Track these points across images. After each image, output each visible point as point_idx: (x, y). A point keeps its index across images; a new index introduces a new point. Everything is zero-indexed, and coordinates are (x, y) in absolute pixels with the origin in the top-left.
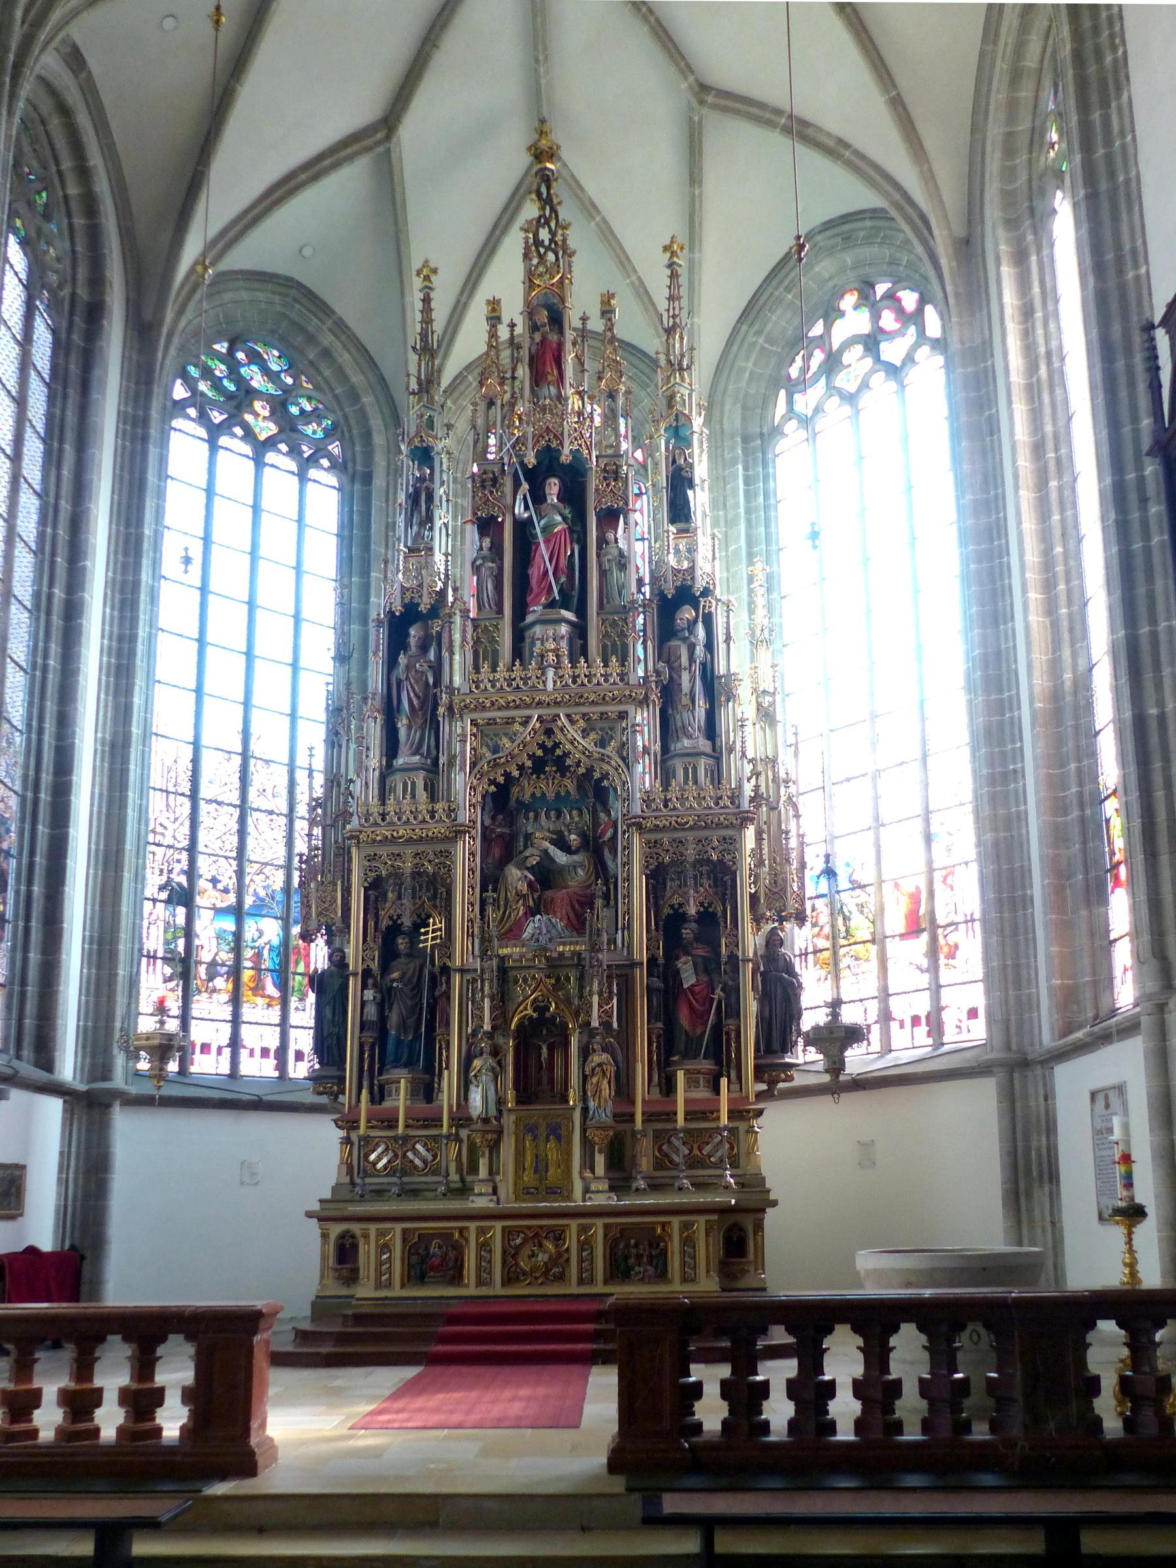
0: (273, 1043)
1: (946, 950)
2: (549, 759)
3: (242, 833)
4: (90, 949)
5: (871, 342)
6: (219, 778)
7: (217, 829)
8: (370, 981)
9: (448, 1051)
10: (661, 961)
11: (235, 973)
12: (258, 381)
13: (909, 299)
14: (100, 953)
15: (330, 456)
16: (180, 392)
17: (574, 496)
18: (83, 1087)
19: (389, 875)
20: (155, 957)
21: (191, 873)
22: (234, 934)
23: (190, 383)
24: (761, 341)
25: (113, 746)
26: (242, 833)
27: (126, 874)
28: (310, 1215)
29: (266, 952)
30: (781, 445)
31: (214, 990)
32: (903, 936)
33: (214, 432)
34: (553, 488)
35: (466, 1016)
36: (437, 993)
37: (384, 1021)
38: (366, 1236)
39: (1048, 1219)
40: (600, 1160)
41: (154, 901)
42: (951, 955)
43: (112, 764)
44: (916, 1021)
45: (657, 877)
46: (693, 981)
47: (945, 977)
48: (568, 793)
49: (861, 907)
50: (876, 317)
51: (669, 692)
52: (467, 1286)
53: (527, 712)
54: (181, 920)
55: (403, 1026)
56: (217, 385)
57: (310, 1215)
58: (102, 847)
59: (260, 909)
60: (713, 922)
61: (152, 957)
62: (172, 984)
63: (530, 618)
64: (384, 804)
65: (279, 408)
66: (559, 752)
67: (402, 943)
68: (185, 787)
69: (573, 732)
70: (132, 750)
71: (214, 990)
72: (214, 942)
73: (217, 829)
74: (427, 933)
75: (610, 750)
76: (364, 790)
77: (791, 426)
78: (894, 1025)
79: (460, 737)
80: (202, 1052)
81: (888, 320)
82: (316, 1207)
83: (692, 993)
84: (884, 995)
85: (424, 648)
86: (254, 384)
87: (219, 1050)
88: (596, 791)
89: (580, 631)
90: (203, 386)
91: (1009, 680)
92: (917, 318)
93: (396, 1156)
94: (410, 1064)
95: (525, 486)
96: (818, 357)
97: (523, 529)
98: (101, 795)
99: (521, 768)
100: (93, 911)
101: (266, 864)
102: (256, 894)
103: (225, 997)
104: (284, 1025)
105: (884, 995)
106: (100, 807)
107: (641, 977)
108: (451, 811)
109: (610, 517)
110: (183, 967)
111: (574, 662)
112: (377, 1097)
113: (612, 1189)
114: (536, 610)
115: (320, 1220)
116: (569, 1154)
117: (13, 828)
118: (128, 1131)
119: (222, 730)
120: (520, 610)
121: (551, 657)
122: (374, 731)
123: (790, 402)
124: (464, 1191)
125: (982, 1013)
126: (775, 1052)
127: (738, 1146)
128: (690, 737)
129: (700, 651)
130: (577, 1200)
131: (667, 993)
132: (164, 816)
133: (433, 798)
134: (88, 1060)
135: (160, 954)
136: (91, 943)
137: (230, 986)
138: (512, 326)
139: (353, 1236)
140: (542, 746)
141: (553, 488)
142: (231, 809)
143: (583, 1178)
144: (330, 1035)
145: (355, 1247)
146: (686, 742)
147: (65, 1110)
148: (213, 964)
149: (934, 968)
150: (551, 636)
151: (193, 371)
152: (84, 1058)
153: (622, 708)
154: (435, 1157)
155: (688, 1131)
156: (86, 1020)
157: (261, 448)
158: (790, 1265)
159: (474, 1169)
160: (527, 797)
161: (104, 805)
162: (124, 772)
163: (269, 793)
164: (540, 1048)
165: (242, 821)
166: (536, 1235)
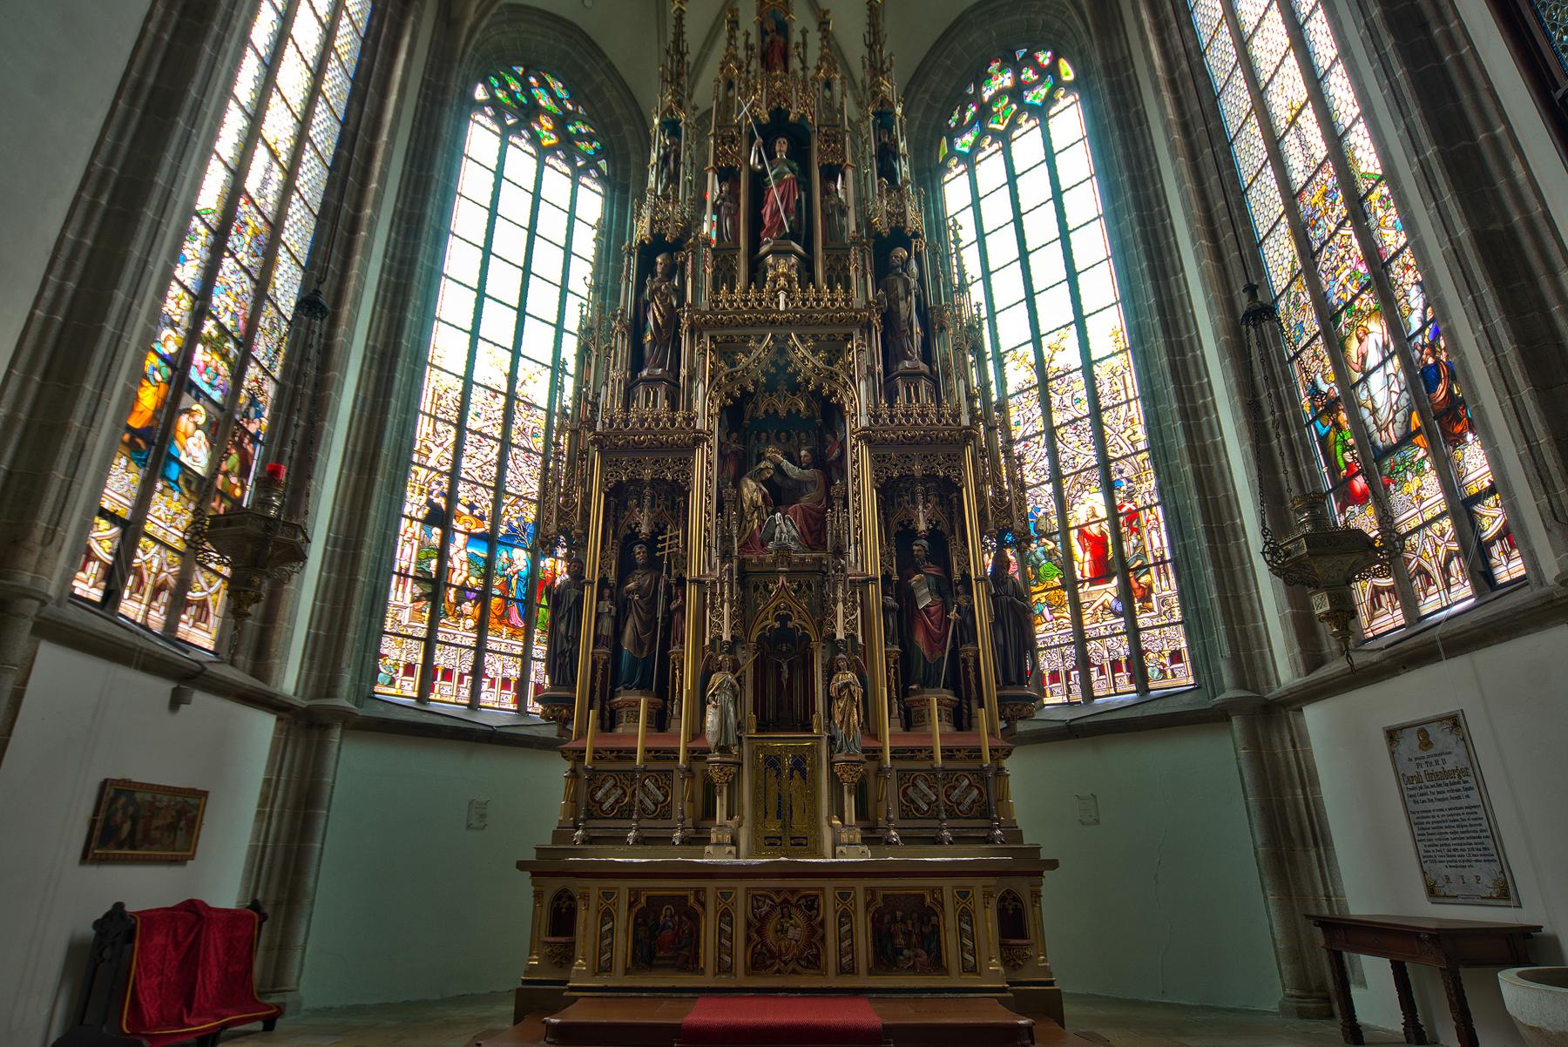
0: (514, 673)
1: (1139, 592)
3: (502, 465)
4: (333, 552)
5: (1016, 92)
6: (485, 413)
7: (479, 459)
8: (607, 592)
9: (682, 672)
10: (896, 578)
11: (483, 597)
12: (545, 101)
13: (1044, 58)
14: (343, 556)
15: (598, 169)
16: (480, 93)
17: (800, 154)
18: (305, 703)
19: (630, 481)
20: (406, 576)
21: (451, 496)
22: (485, 560)
23: (490, 89)
24: (927, 97)
25: (383, 354)
26: (502, 465)
27: (379, 478)
28: (522, 865)
29: (514, 582)
31: (461, 615)
32: (1093, 582)
33: (505, 134)
36: (673, 606)
37: (615, 635)
38: (585, 897)
39: (1322, 892)
40: (850, 803)
41: (412, 519)
42: (1146, 598)
43: (380, 371)
44: (1116, 666)
45: (889, 493)
46: (928, 601)
47: (1143, 620)
48: (799, 411)
49: (1049, 555)
50: (1017, 73)
52: (702, 972)
53: (762, 331)
54: (436, 540)
55: (638, 643)
56: (511, 95)
57: (522, 865)
58: (359, 449)
59: (511, 540)
60: (944, 542)
61: (404, 575)
62: (421, 604)
63: (764, 249)
64: (628, 411)
65: (560, 123)
66: (790, 370)
67: (639, 553)
68: (453, 416)
69: (802, 351)
70: (400, 361)
71: (461, 615)
72: (465, 567)
73: (479, 459)
74: (664, 540)
75: (836, 368)
76: (610, 398)
78: (1094, 671)
79: (696, 356)
80: (443, 679)
81: (1028, 75)
82: (531, 856)
83: (927, 612)
84: (1080, 639)
85: (669, 275)
86: (542, 102)
87: (461, 676)
89: (807, 266)
90: (500, 94)
91: (1186, 323)
92: (1053, 69)
93: (625, 794)
94: (644, 686)
95: (759, 140)
98: (365, 399)
99: (755, 383)
100: (341, 512)
101: (521, 497)
102: (509, 524)
103: (470, 623)
104: (526, 658)
105: (1080, 639)
106: (362, 410)
108: (689, 420)
110: (434, 587)
111: (804, 288)
112: (607, 724)
113: (865, 841)
115: (534, 874)
116: (814, 797)
117: (266, 413)
118: (351, 764)
119: (491, 368)
120: (755, 243)
121: (782, 281)
122: (622, 345)
123: (951, 144)
124: (698, 839)
125: (1186, 656)
126: (1012, 684)
128: (910, 359)
129: (913, 282)
131: (903, 615)
132: (431, 442)
133: (674, 407)
134: (314, 673)
135: (411, 573)
136: (335, 545)
137: (477, 613)
138: (748, 34)
139: (571, 898)
140: (774, 364)
141: (781, 147)
142: (492, 442)
143: (831, 825)
144: (563, 652)
145: (572, 912)
146: (907, 363)
147: (278, 730)
148: (462, 588)
149: (1130, 615)
150: (782, 267)
151: (493, 81)
152: (310, 670)
153: (847, 330)
154: (666, 796)
155: (943, 769)
156: (318, 628)
157: (542, 154)
159: (709, 813)
160: (761, 413)
161: (367, 408)
162: (390, 379)
163: (529, 432)
164: (779, 666)
165: (503, 456)
166: (786, 901)
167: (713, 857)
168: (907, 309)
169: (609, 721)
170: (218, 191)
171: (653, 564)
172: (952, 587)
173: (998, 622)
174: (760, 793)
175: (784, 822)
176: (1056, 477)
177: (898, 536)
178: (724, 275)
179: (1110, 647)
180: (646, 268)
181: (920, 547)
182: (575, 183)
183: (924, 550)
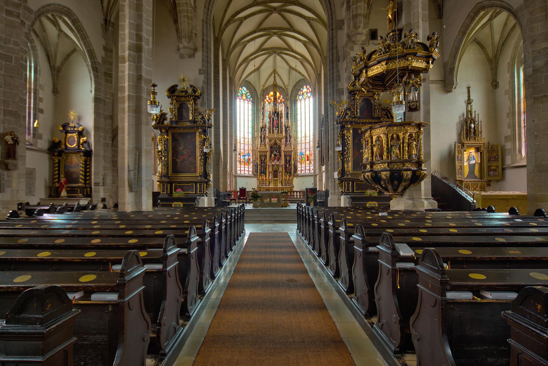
2: (275, 144)
35: (269, 169)
45: (285, 156)
51: (286, 137)
60: (290, 161)
79: (267, 140)
97: (273, 119)
109: (281, 118)
110: (240, 161)
127: (292, 183)
131: (286, 168)
141: (276, 114)
150: (276, 131)
157: (244, 100)
158: (294, 189)
168: (288, 136)
172: (290, 165)
175: (275, 184)
176: (305, 149)
177: (286, 160)
178: (270, 132)
179: (308, 168)
180: (262, 130)
183: (288, 162)
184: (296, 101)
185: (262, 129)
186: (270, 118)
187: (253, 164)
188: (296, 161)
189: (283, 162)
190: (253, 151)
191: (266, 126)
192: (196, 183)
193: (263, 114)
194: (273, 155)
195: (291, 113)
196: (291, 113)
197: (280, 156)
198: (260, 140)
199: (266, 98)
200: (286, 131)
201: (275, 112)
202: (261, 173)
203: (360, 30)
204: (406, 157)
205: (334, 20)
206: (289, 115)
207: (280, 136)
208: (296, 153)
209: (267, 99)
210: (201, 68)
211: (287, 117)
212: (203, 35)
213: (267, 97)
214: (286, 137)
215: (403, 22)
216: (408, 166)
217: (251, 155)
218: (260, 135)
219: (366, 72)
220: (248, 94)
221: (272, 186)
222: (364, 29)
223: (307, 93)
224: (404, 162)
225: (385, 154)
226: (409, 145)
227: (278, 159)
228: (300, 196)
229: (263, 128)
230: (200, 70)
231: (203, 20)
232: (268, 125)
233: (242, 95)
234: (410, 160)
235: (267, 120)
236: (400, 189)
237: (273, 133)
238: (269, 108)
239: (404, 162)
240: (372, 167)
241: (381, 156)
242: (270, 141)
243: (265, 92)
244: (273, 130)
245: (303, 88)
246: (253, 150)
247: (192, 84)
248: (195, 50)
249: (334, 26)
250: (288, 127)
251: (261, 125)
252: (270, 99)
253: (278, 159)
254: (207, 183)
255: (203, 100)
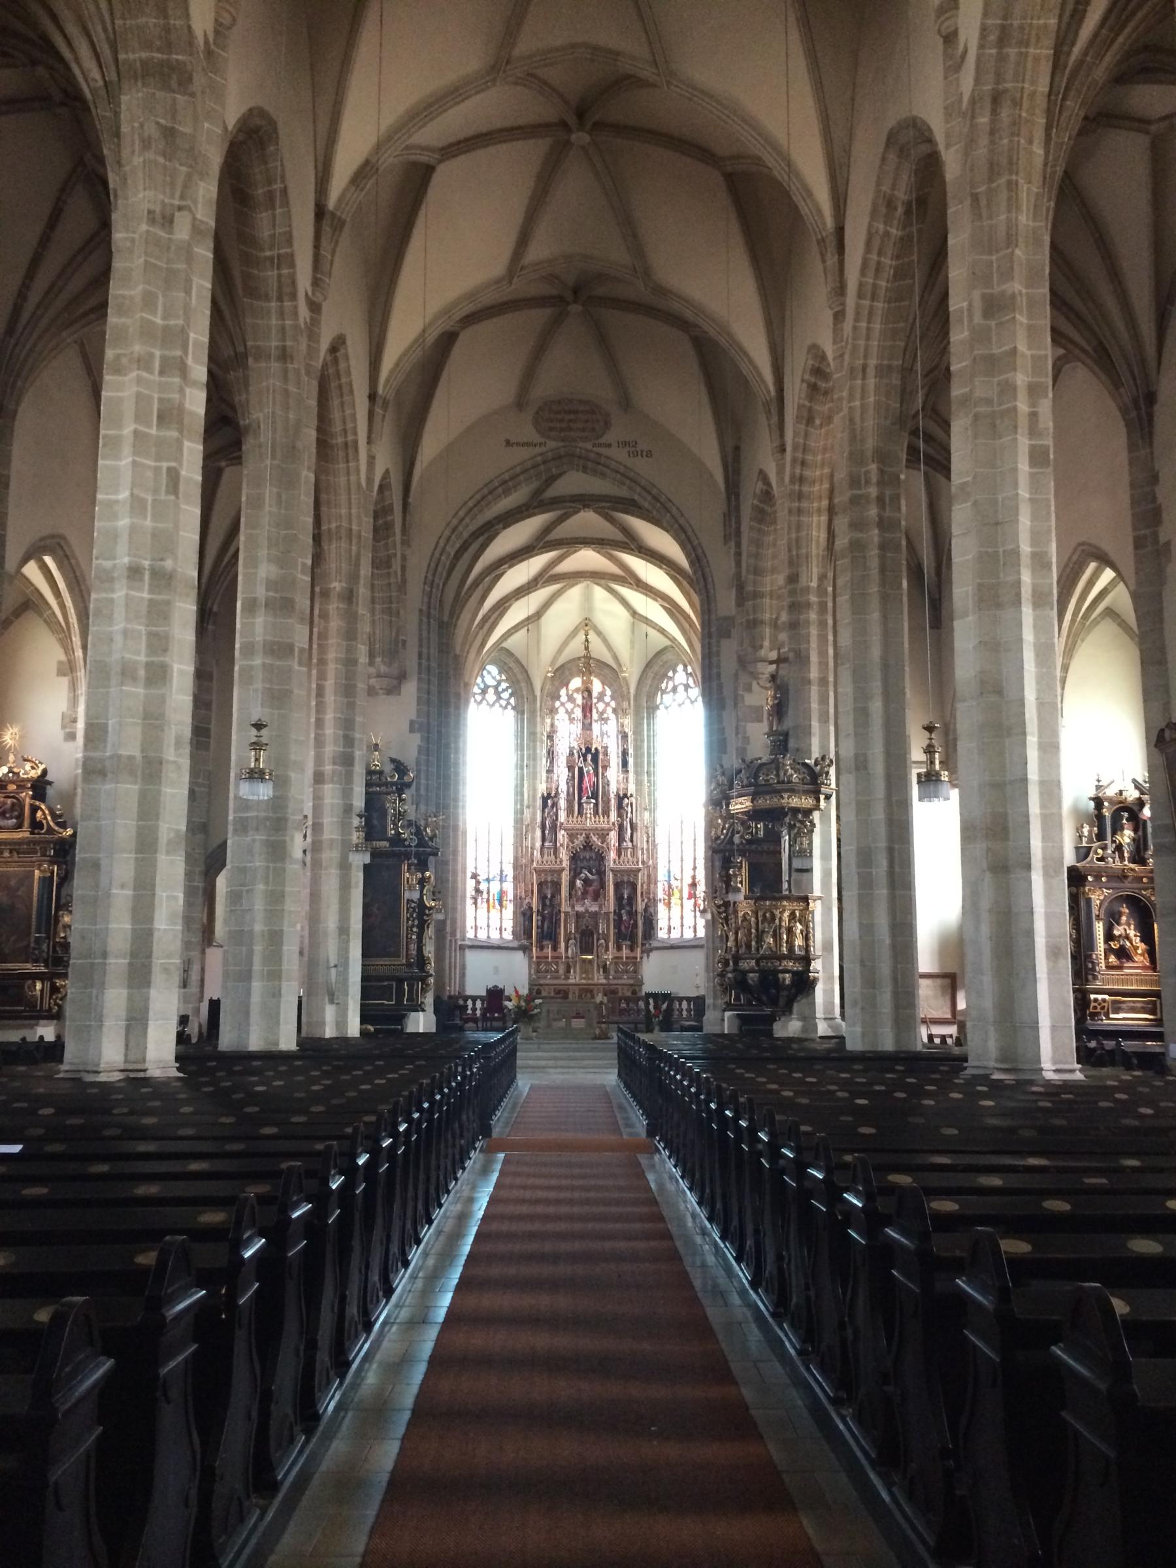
2: (588, 846)
30: (658, 713)
34: (589, 757)
45: (617, 886)
51: (621, 828)
60: (632, 899)
77: (661, 707)
79: (562, 836)
85: (552, 807)
88: (601, 857)
94: (550, 939)
96: (671, 685)
97: (581, 769)
107: (612, 916)
109: (605, 768)
114: (584, 799)
120: (580, 798)
130: (596, 981)
131: (619, 922)
141: (589, 757)
150: (589, 808)
167: (571, 981)
168: (627, 824)
169: (542, 948)
170: (512, 842)
171: (552, 905)
172: (632, 914)
173: (644, 924)
174: (581, 968)
177: (619, 898)
178: (570, 811)
180: (545, 805)
181: (625, 902)
182: (651, 950)
183: (626, 901)
184: (652, 709)
185: (544, 800)
186: (570, 768)
187: (515, 906)
188: (652, 902)
189: (611, 904)
190: (515, 867)
191: (557, 794)
192: (400, 981)
193: (551, 754)
194: (579, 883)
195: (638, 748)
196: (638, 748)
197: (603, 885)
198: (538, 833)
199: (558, 697)
200: (620, 807)
201: (588, 750)
202: (542, 937)
203: (763, 653)
204: (785, 950)
205: (713, 617)
206: (631, 761)
207: (602, 822)
208: (652, 880)
209: (564, 698)
210: (414, 717)
211: (625, 764)
212: (421, 646)
213: (563, 692)
214: (621, 828)
215: (788, 723)
216: (790, 964)
217: (510, 878)
218: (539, 819)
219: (727, 806)
220: (504, 685)
221: (575, 978)
222: (771, 650)
223: (687, 687)
224: (782, 957)
225: (753, 943)
226: (790, 931)
227: (596, 897)
228: (689, 1010)
229: (549, 800)
230: (412, 723)
231: (421, 611)
232: (563, 787)
233: (484, 692)
234: (791, 955)
235: (562, 773)
236: (782, 1002)
237: (580, 813)
238: (568, 735)
239: (782, 957)
240: (736, 963)
241: (749, 946)
242: (572, 837)
243: (561, 674)
244: (580, 805)
245: (675, 672)
246: (517, 866)
247: (393, 756)
248: (402, 677)
249: (713, 629)
250: (625, 796)
251: (542, 788)
252: (571, 699)
253: (596, 897)
254: (424, 980)
255: (418, 790)
